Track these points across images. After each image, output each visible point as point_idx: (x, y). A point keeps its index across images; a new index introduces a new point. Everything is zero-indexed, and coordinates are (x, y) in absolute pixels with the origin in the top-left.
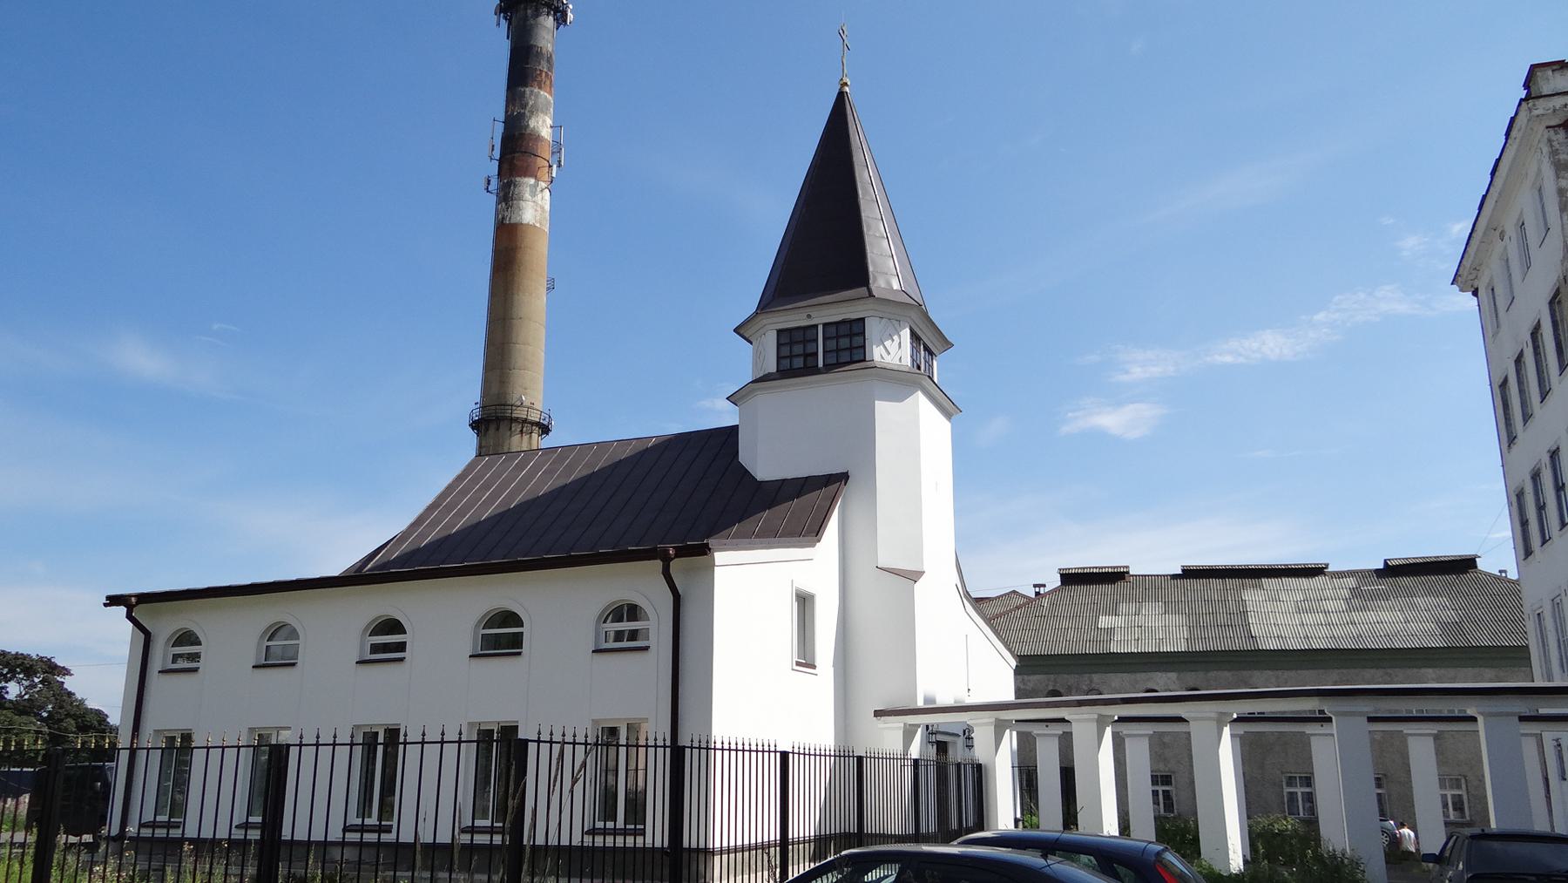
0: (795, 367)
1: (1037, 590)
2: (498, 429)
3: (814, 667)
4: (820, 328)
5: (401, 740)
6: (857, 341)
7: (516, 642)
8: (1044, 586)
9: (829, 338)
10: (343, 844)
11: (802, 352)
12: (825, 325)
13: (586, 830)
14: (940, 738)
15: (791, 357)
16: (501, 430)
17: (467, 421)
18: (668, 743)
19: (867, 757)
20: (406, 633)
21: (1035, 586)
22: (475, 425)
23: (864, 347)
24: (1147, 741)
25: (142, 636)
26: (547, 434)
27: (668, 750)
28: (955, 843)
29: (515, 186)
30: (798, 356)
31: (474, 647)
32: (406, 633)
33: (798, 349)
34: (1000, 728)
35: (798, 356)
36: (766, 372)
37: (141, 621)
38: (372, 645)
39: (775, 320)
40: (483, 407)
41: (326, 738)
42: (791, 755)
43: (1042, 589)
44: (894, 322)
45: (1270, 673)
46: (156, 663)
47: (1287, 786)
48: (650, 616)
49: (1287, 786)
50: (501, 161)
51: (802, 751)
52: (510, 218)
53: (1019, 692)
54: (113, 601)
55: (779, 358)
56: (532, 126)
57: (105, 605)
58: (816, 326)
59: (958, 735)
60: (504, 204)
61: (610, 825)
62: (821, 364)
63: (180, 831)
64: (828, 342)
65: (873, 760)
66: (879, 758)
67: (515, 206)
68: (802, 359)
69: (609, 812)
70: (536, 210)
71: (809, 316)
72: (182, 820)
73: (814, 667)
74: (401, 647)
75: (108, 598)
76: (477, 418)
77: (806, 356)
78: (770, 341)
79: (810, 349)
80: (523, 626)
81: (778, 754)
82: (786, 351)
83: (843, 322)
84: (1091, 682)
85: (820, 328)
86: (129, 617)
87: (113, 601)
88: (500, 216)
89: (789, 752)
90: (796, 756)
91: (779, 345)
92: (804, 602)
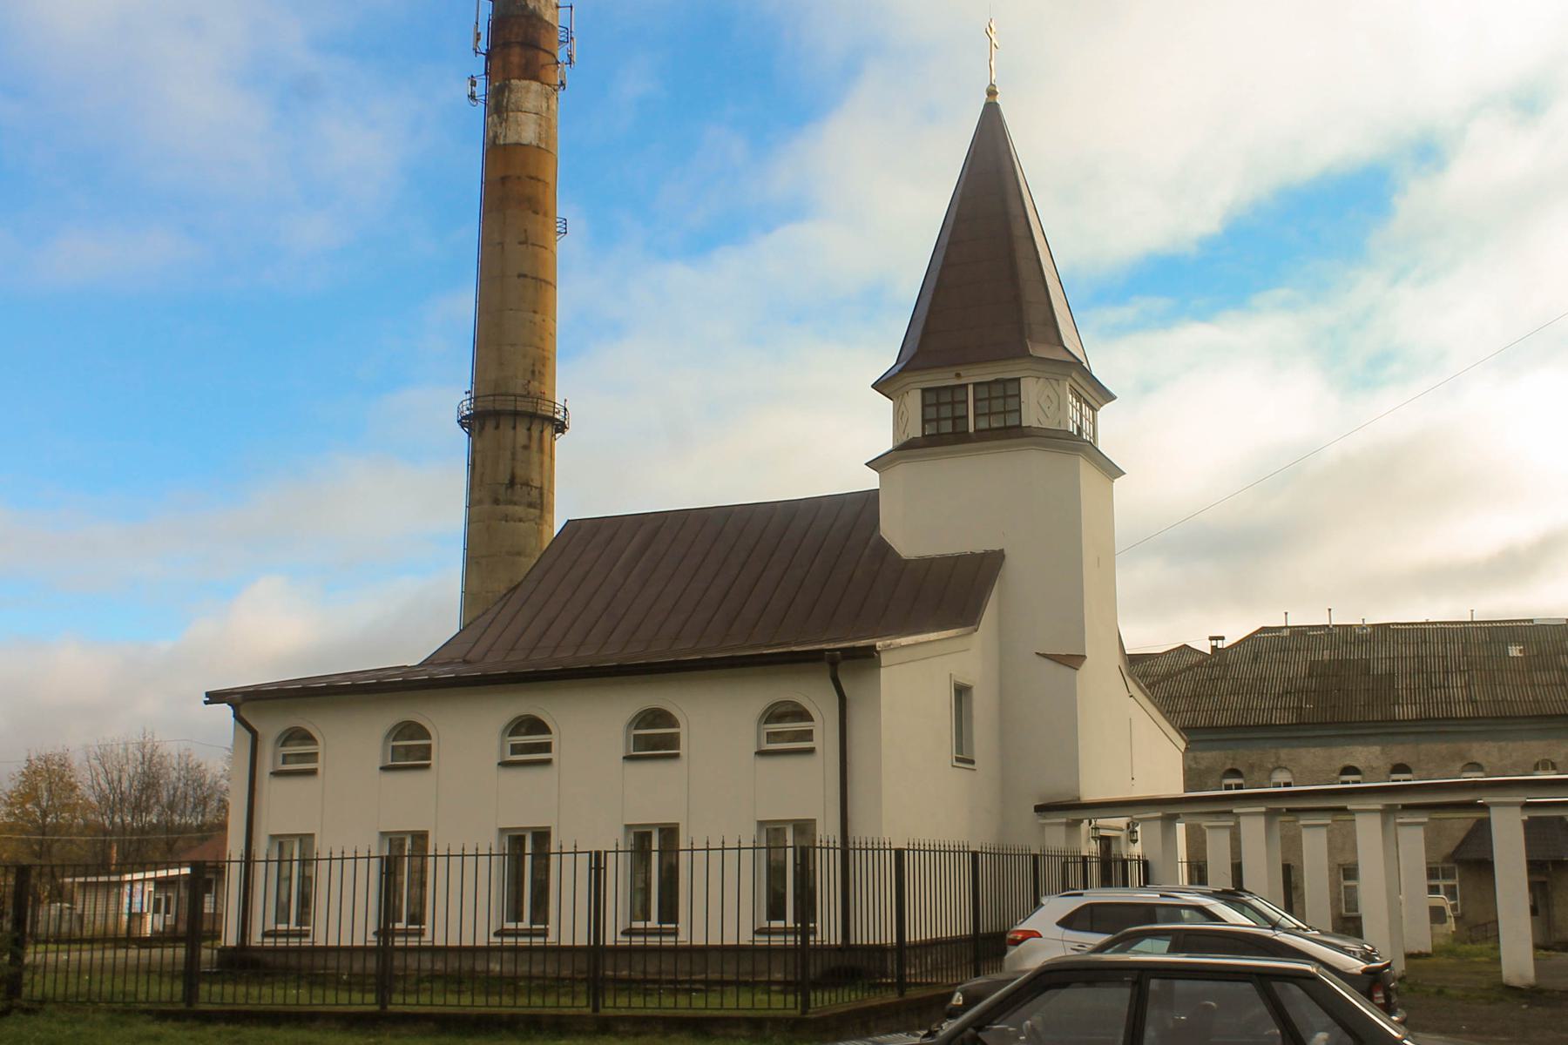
0: (943, 431)
1: (1214, 643)
2: (497, 427)
3: (972, 762)
4: (971, 388)
5: (227, 859)
6: (1012, 403)
7: (672, 742)
8: (1222, 638)
9: (981, 400)
10: (488, 950)
11: (950, 415)
12: (976, 385)
13: (756, 929)
14: (1103, 833)
15: (938, 420)
16: (501, 427)
17: (454, 417)
18: (838, 845)
19: (909, 850)
20: (551, 733)
21: (1211, 638)
22: (464, 422)
23: (1019, 410)
24: (1325, 833)
25: (249, 736)
26: (563, 433)
27: (506, 857)
28: (1109, 951)
29: (510, 91)
30: (946, 419)
31: (627, 748)
32: (551, 733)
33: (946, 411)
34: (1170, 820)
35: (946, 419)
36: (910, 437)
37: (253, 726)
38: (512, 745)
39: (919, 378)
40: (476, 399)
41: (470, 850)
42: (906, 852)
43: (1220, 642)
44: (1053, 382)
45: (1491, 744)
46: (266, 764)
47: (1345, 879)
48: (814, 717)
49: (1345, 879)
50: (489, 56)
51: (937, 849)
52: (505, 136)
53: (1192, 777)
54: (214, 697)
55: (925, 421)
56: (531, 6)
57: (206, 703)
58: (966, 386)
59: (1122, 830)
60: (495, 116)
61: (780, 924)
62: (971, 429)
63: (310, 940)
64: (979, 404)
65: (927, 853)
66: (940, 851)
67: (511, 119)
68: (950, 422)
69: (776, 911)
70: (540, 125)
71: (958, 376)
72: (311, 928)
73: (972, 762)
74: (547, 747)
75: (208, 694)
76: (468, 413)
77: (954, 419)
78: (914, 400)
79: (959, 412)
80: (679, 727)
81: (893, 852)
82: (932, 413)
83: (997, 381)
84: (1278, 758)
85: (971, 388)
86: (237, 717)
87: (214, 697)
88: (491, 134)
89: (904, 849)
90: (911, 852)
91: (924, 406)
92: (962, 692)
